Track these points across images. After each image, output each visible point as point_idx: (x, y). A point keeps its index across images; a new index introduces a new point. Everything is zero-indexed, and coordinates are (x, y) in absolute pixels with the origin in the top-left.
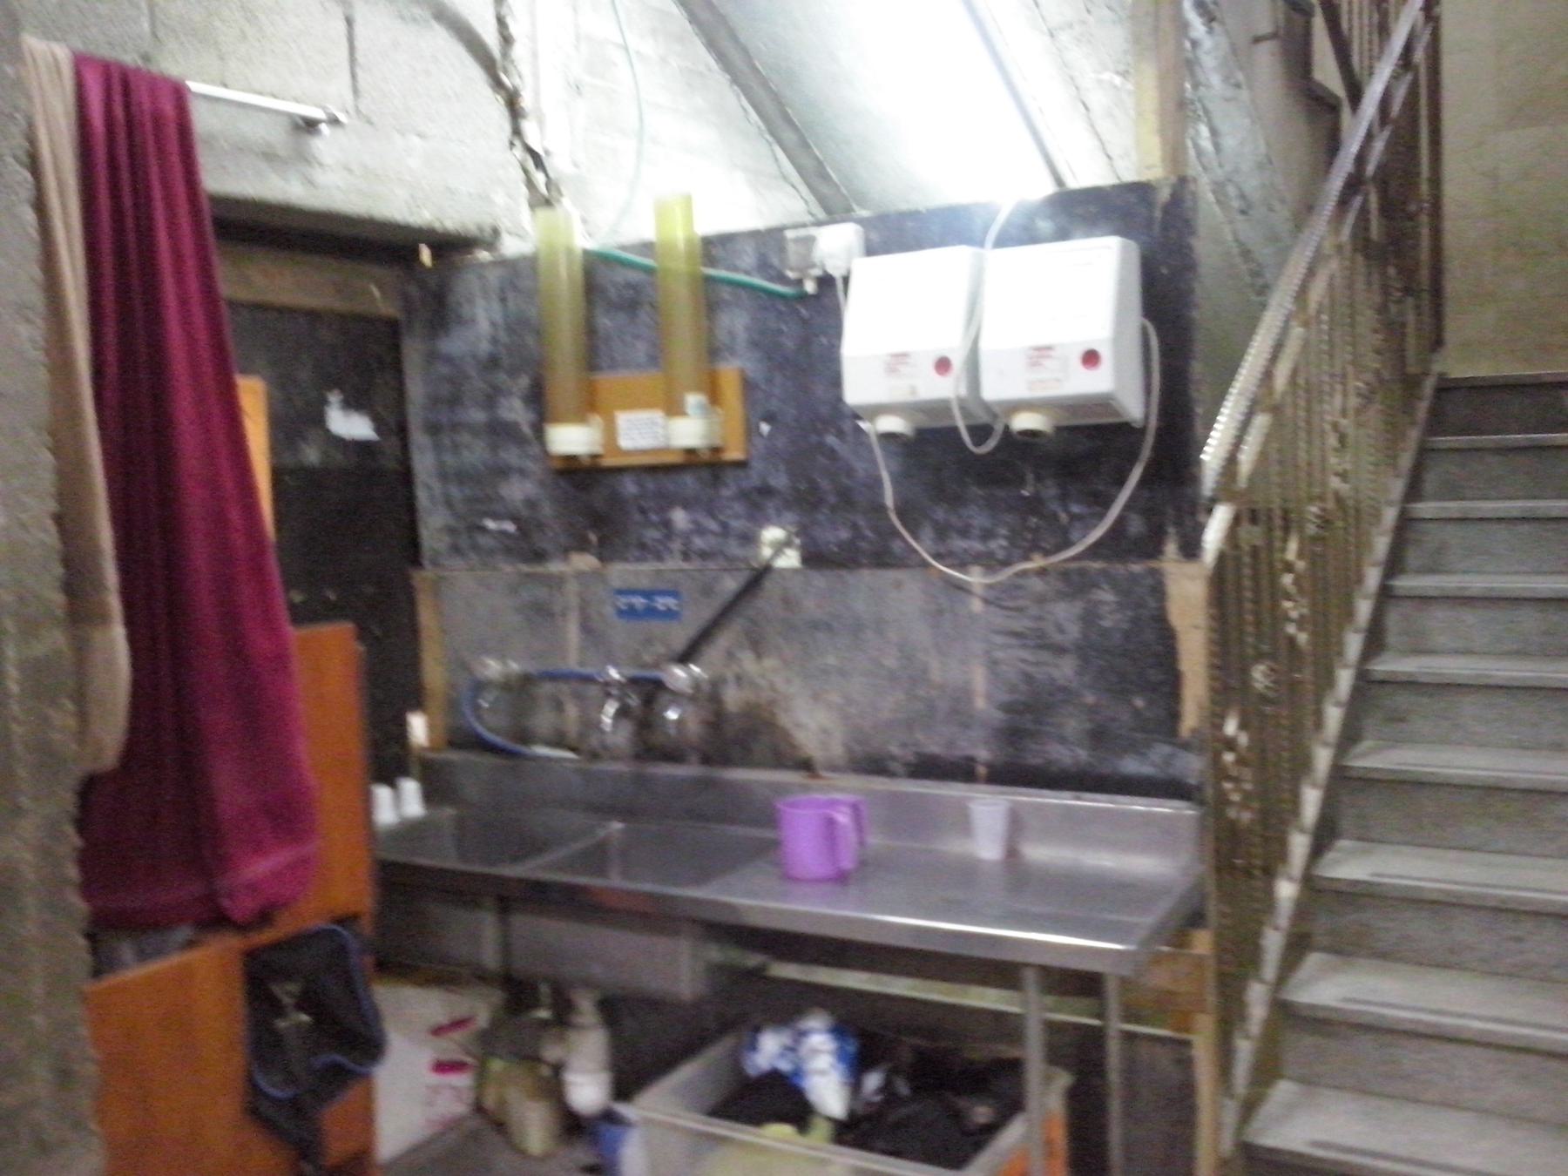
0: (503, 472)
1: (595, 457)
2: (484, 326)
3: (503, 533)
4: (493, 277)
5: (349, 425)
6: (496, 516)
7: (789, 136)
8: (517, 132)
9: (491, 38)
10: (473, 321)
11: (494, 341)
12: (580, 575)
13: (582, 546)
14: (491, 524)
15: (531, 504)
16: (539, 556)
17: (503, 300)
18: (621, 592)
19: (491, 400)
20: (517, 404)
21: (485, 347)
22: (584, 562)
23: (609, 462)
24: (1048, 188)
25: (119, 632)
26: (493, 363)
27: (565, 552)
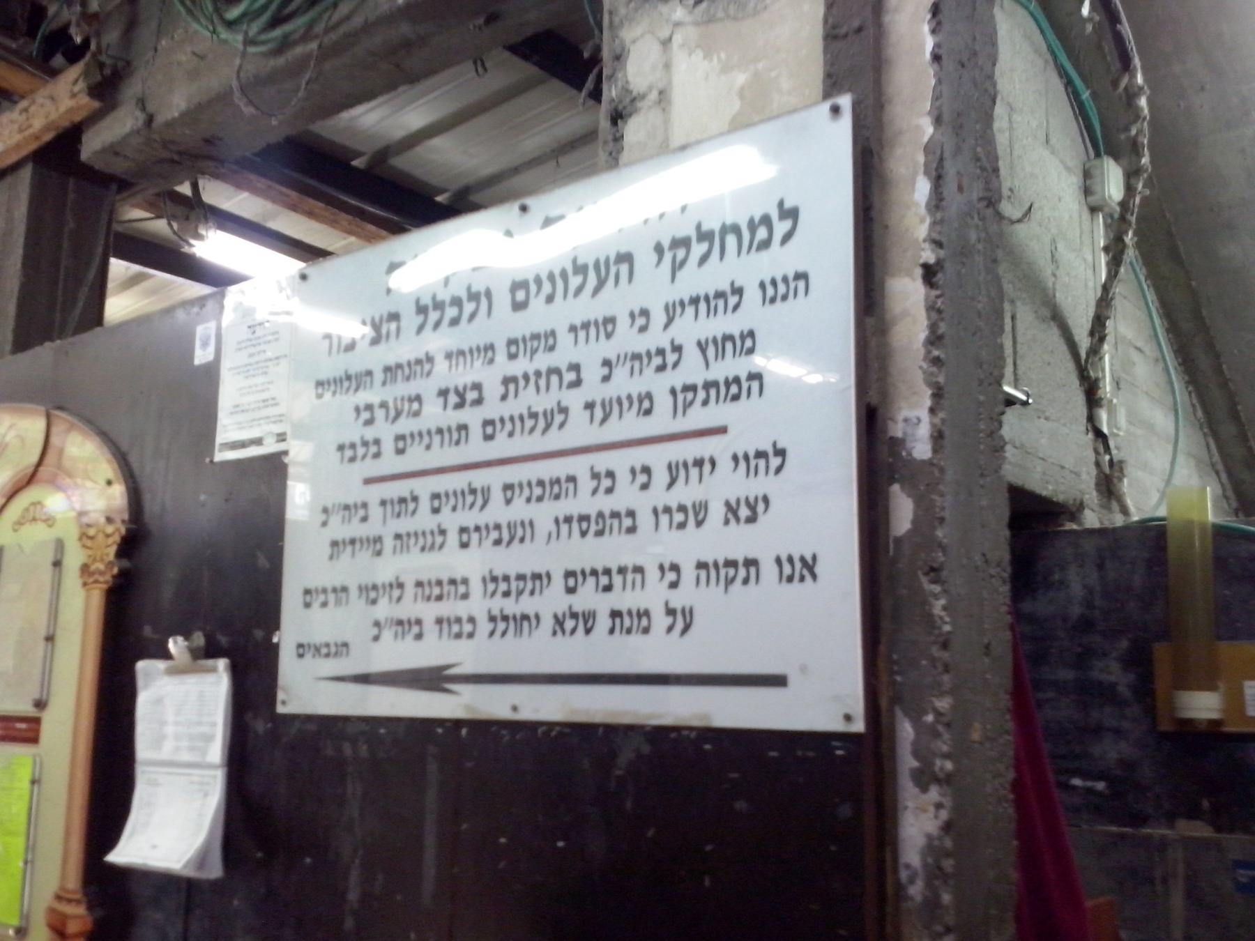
0: (1098, 731)
1: (1215, 723)
2: (1076, 589)
3: (1090, 791)
4: (1089, 546)
5: (930, 718)
6: (1085, 775)
7: (1229, 429)
8: (1091, 418)
9: (1084, 343)
10: (1062, 584)
11: (1089, 605)
12: (1187, 842)
13: (1193, 814)
14: (1077, 782)
15: (1128, 765)
16: (1139, 819)
17: (1101, 567)
18: (1239, 864)
19: (1083, 659)
20: (1115, 667)
21: (1076, 610)
22: (1200, 830)
23: (1230, 729)
24: (70, 493)
25: (1126, 24)
26: (1086, 625)
27: (1171, 818)
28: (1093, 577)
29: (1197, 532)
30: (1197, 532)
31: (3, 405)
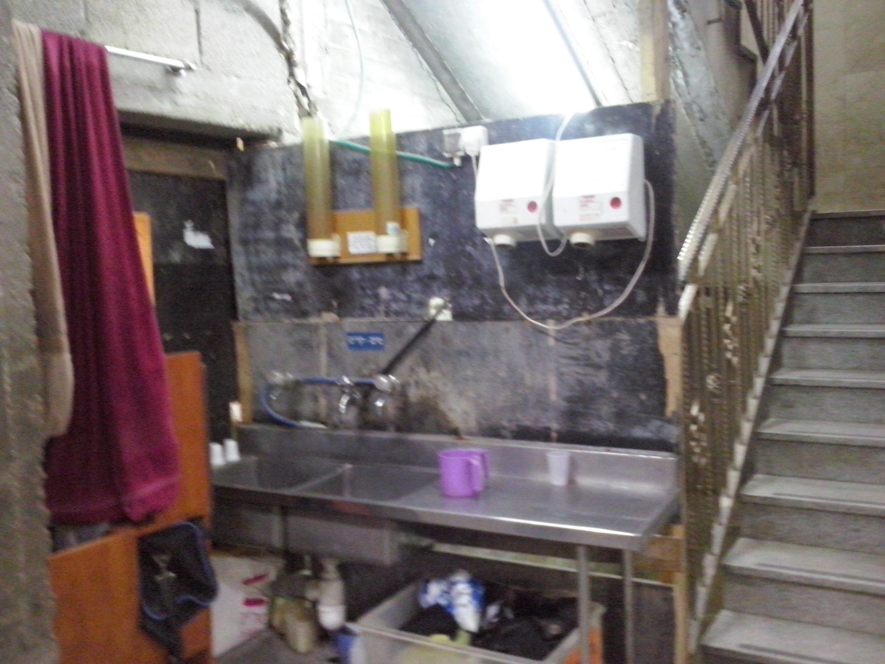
0: (284, 266)
1: (336, 258)
2: (273, 184)
3: (284, 301)
4: (278, 156)
6: (280, 291)
7: (445, 77)
9: (277, 22)
10: (267, 181)
11: (279, 192)
12: (327, 325)
13: (329, 308)
14: (277, 296)
15: (300, 284)
16: (304, 314)
17: (284, 169)
18: (350, 334)
19: (277, 226)
20: (292, 228)
21: (273, 196)
22: (330, 317)
23: (343, 261)
26: (278, 205)
27: (319, 311)
28: (280, 173)
29: (433, 471)
30: (433, 471)
31: (723, 2)
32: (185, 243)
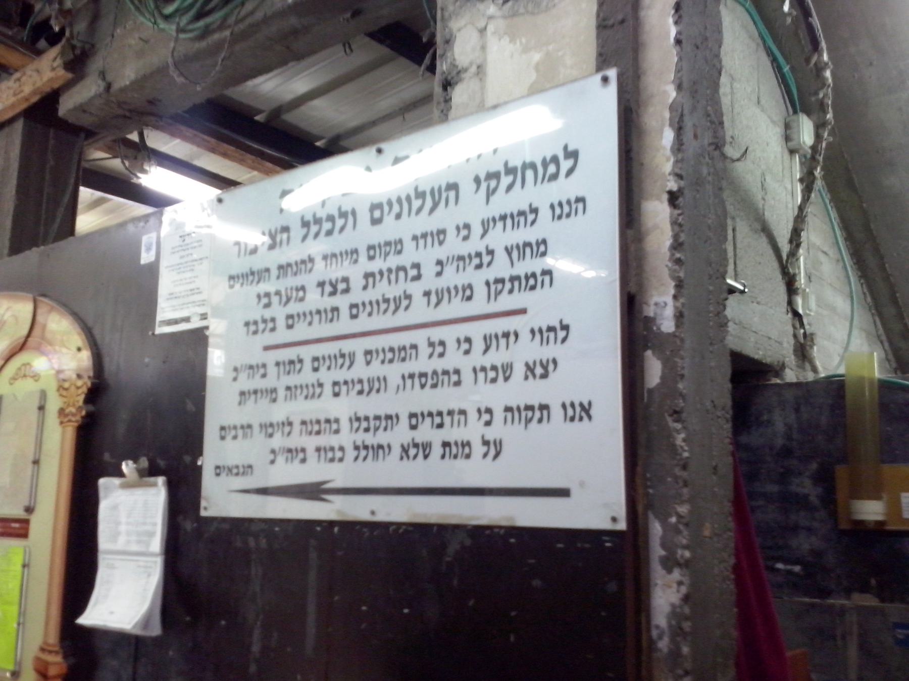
0: (795, 529)
1: (880, 523)
2: (780, 427)
3: (789, 572)
4: (789, 395)
5: (673, 520)
6: (786, 561)
7: (890, 311)
8: (790, 303)
9: (785, 248)
10: (769, 422)
11: (789, 438)
12: (860, 609)
13: (864, 589)
14: (780, 566)
15: (817, 554)
16: (825, 593)
17: (797, 410)
18: (897, 625)
19: (784, 477)
20: (808, 482)
21: (779, 442)
22: (869, 601)
23: (891, 527)
25: (816, 18)
26: (786, 452)
27: (848, 592)
28: (792, 418)
29: (867, 385)
30: (867, 385)
31: (2, 293)
32: (815, 142)
